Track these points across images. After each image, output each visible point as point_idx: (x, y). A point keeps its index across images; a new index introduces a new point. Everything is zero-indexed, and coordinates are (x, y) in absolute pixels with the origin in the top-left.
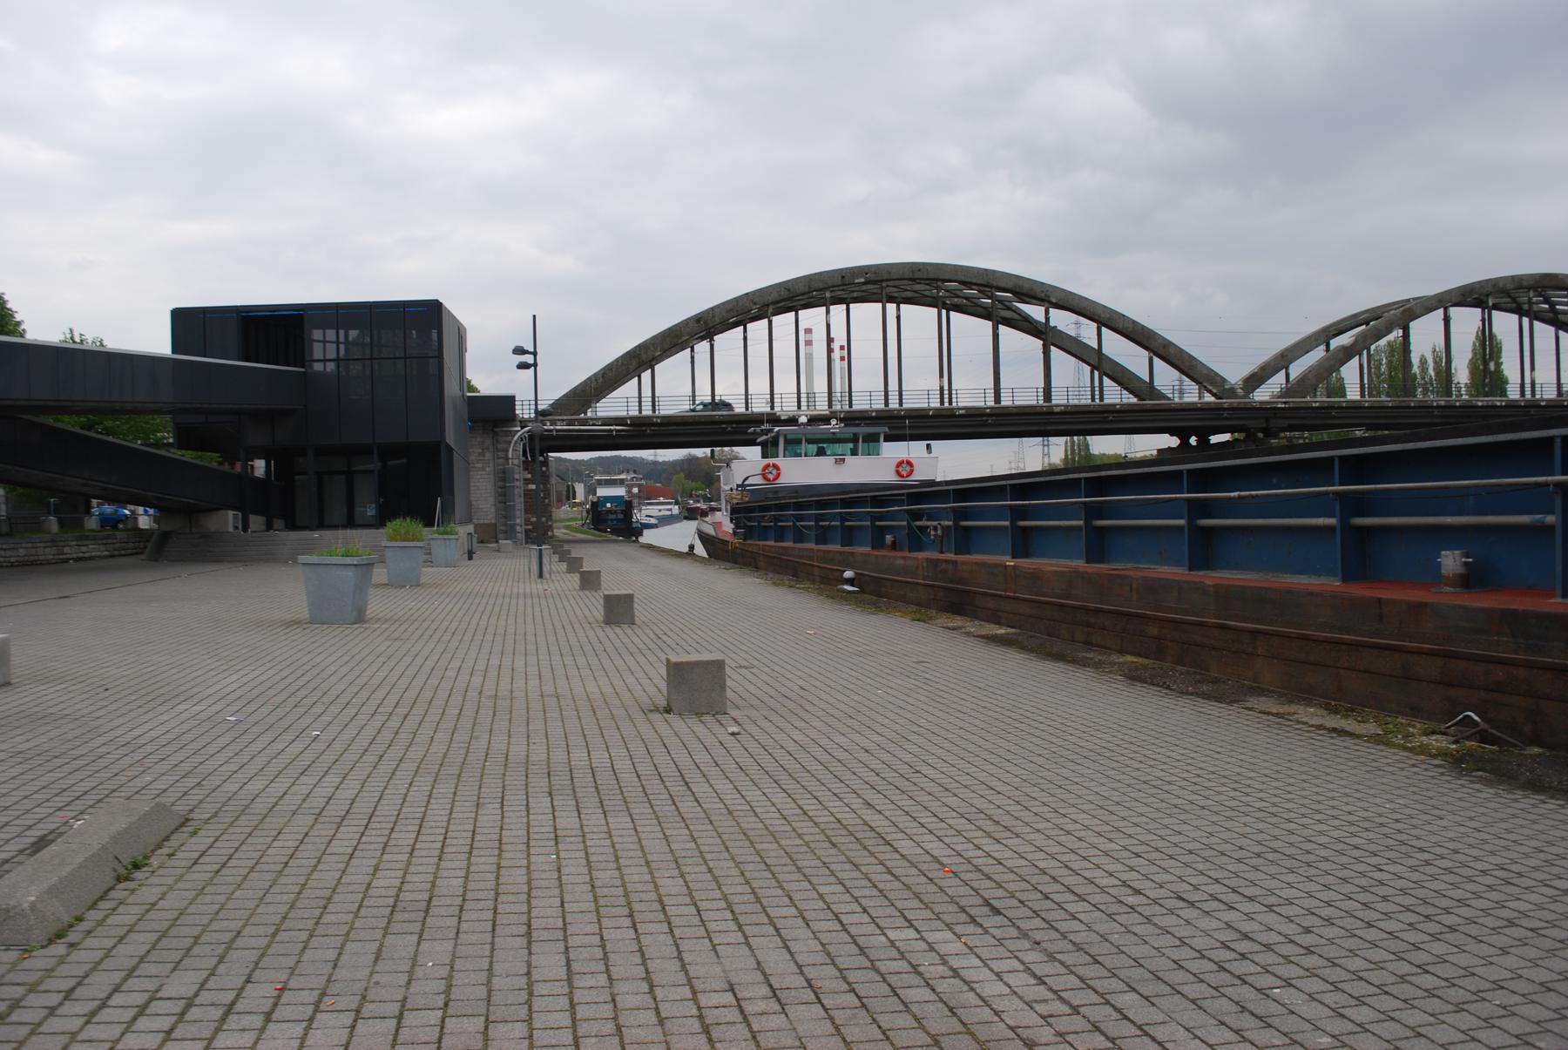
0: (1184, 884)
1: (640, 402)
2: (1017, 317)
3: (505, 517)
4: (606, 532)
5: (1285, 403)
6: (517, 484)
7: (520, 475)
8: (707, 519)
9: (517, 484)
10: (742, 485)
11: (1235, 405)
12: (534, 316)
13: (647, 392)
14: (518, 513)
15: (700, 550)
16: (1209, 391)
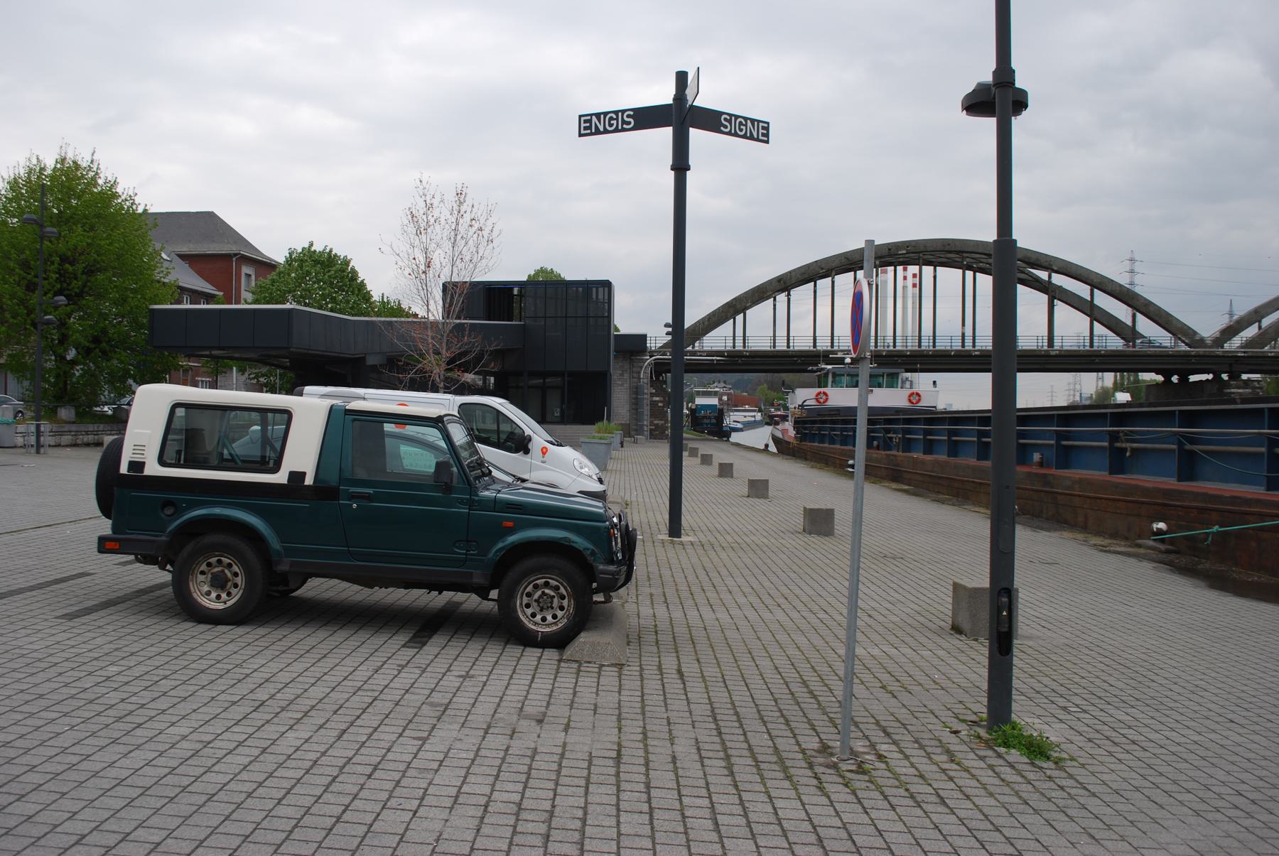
0: (1213, 780)
1: (734, 339)
2: (1030, 278)
3: (636, 420)
4: (703, 432)
5: (1244, 352)
6: (646, 396)
7: (648, 390)
8: (778, 427)
9: (646, 396)
10: (802, 406)
11: (1201, 353)
12: (592, 125)
13: (739, 332)
14: (646, 417)
15: (773, 448)
16: (1183, 342)
